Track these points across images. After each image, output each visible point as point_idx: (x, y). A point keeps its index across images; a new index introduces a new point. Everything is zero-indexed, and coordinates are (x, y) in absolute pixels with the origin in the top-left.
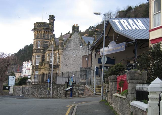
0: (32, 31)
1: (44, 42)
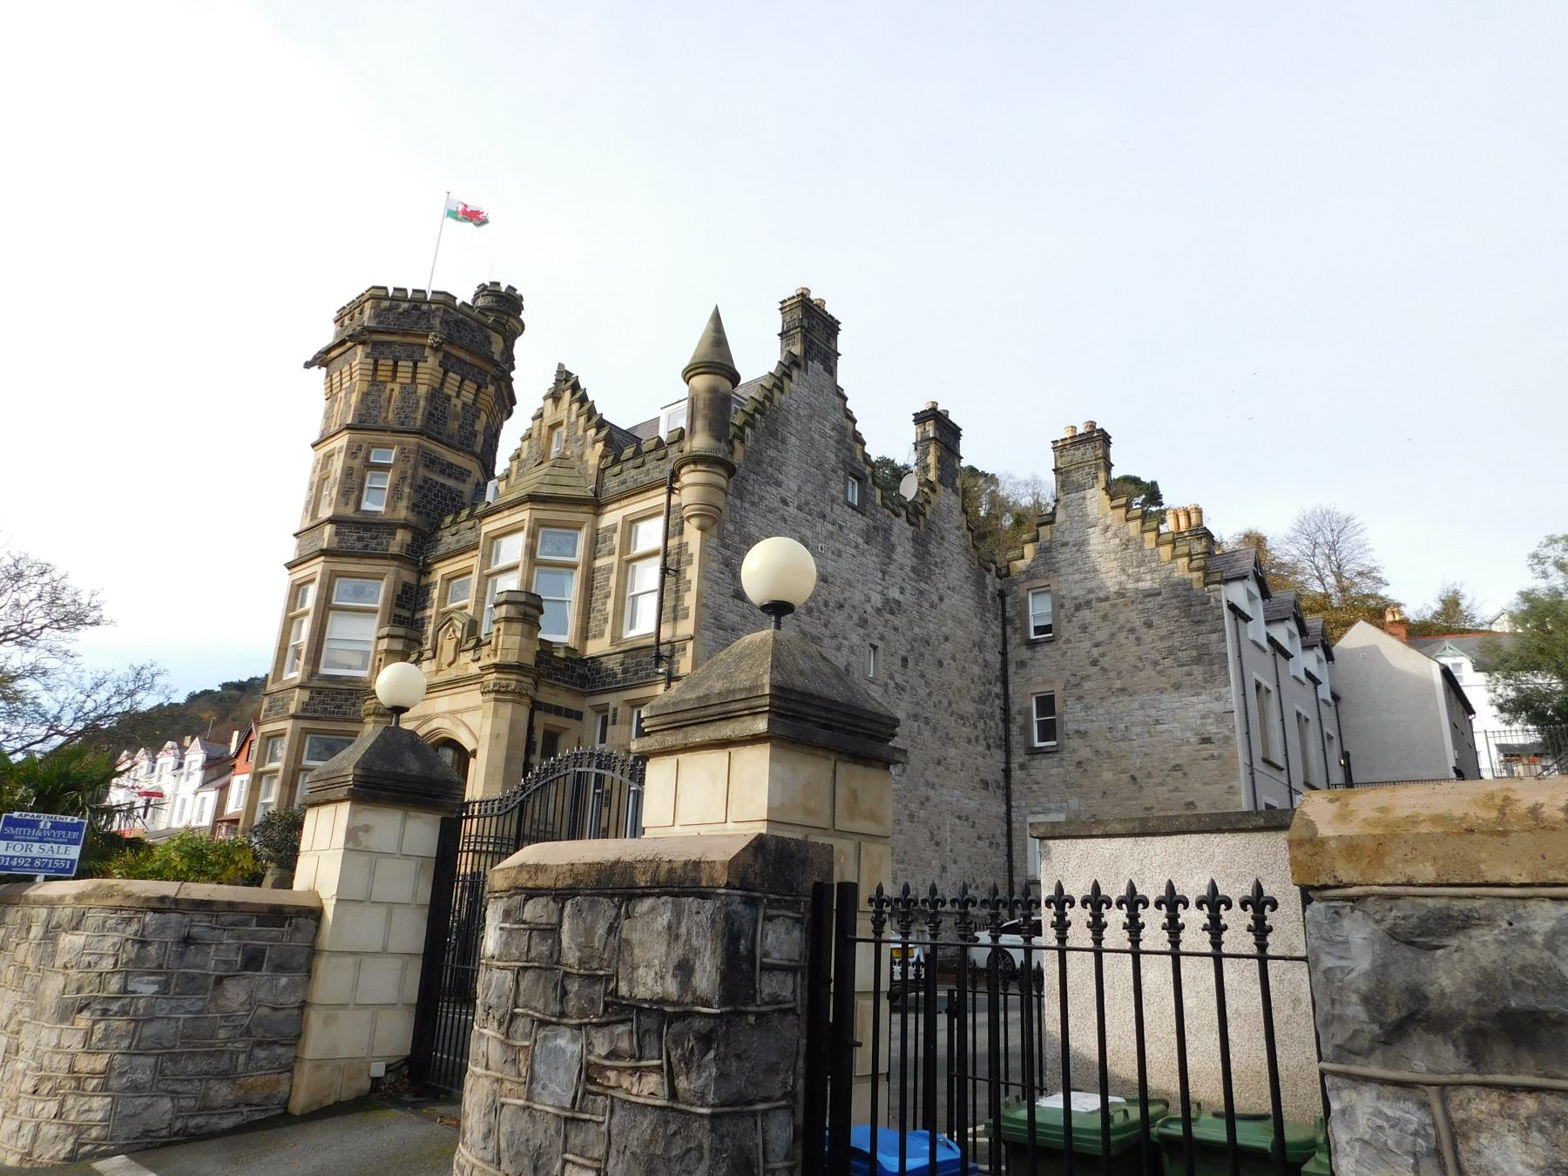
0: (308, 365)
1: (431, 462)
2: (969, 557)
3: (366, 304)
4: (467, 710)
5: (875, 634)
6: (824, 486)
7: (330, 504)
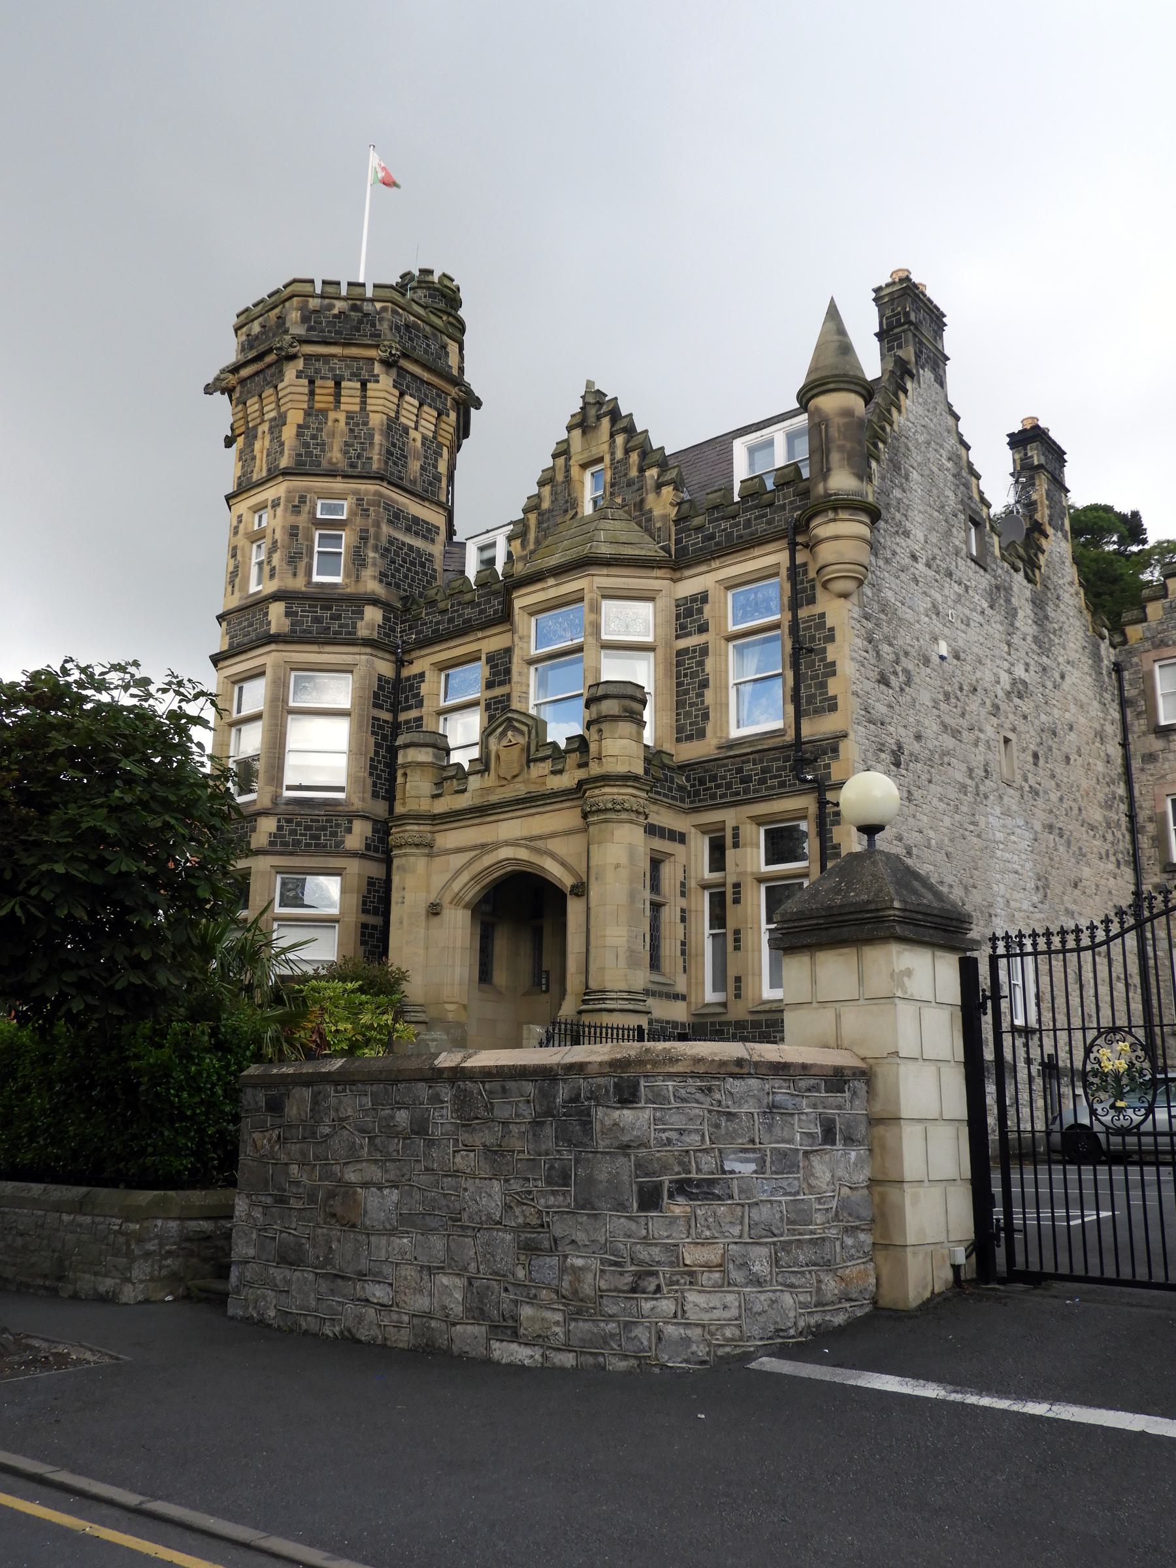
0: (209, 390)
1: (396, 516)
2: (1084, 622)
4: (553, 835)
5: (1007, 725)
6: (948, 534)
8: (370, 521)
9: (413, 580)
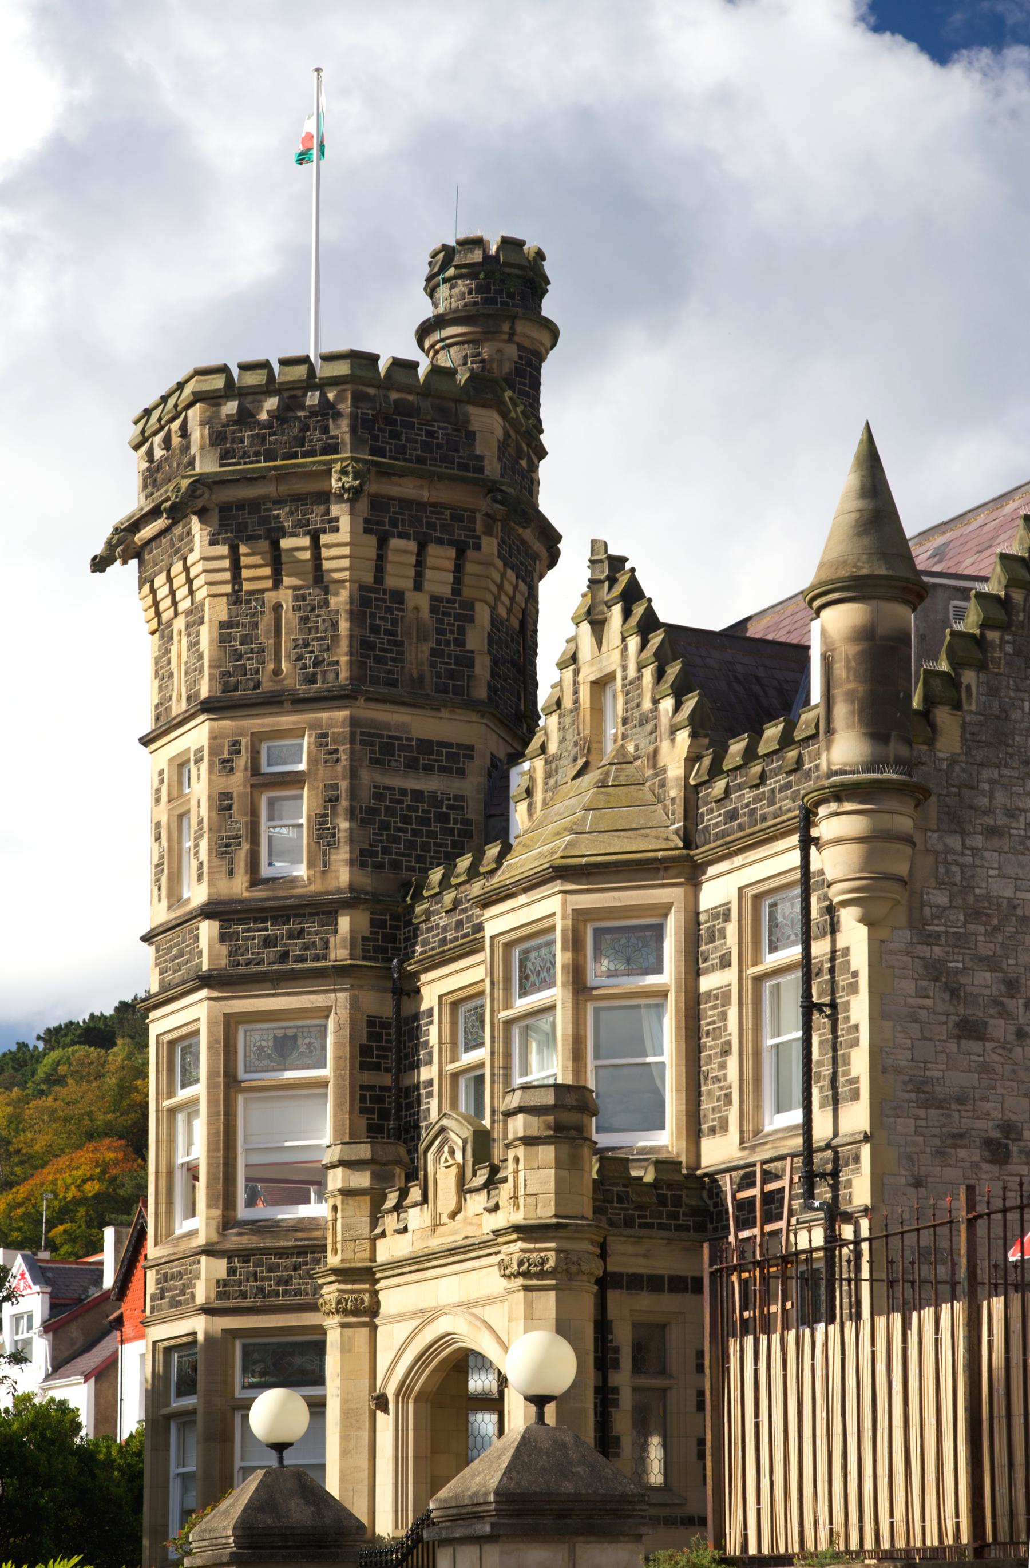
0: (99, 564)
3: (190, 412)
7: (200, 877)
8: (340, 769)
9: (425, 846)
